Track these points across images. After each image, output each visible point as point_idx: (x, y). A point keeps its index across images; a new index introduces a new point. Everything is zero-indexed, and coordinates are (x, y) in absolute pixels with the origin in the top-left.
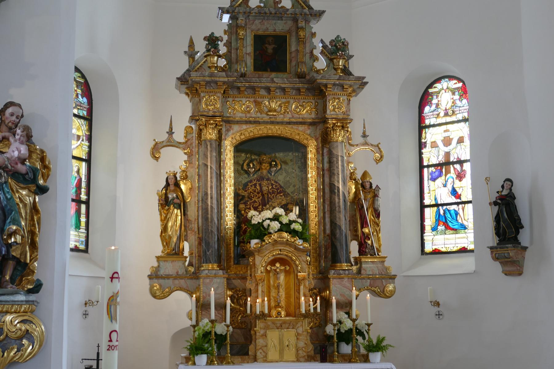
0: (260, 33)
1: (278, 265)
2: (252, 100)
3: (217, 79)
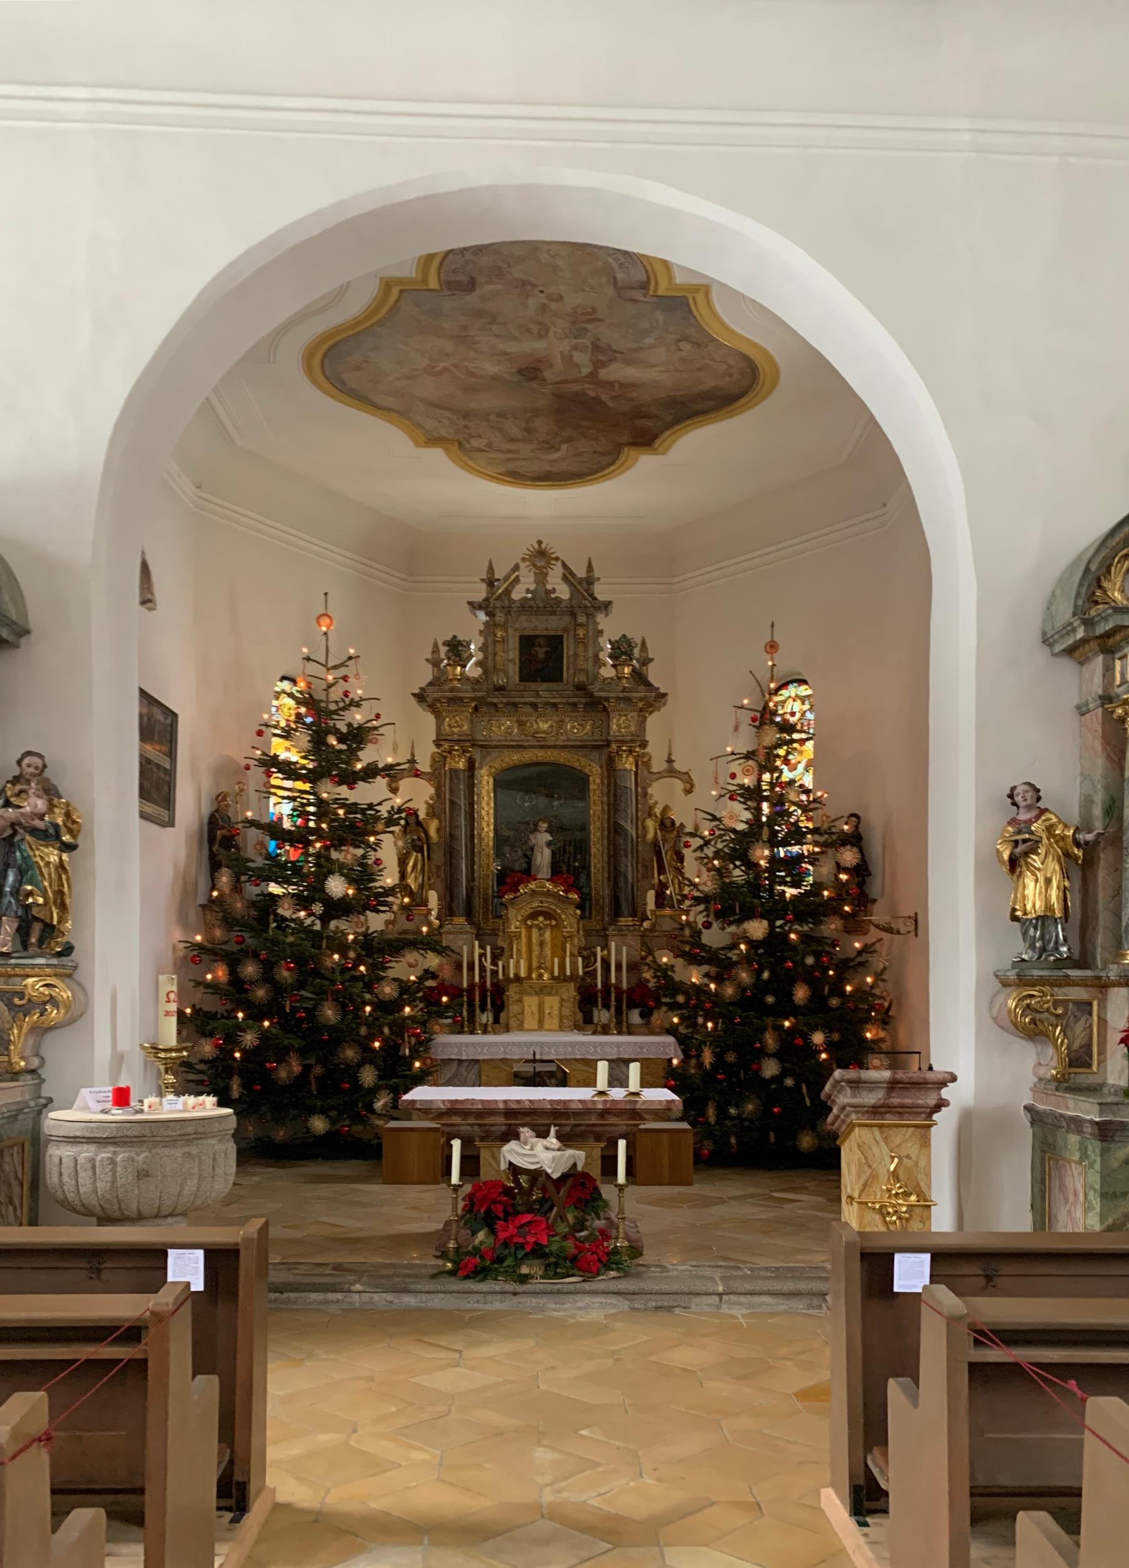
0: (527, 633)
1: (541, 919)
2: (514, 719)
3: (462, 695)
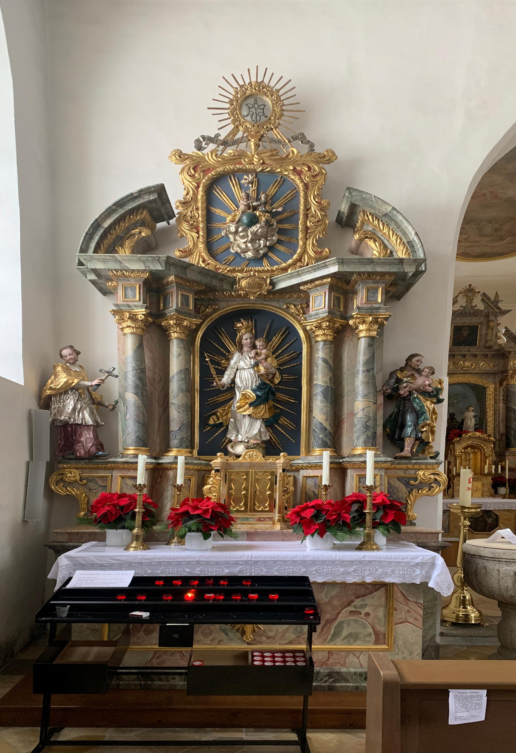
1: (469, 449)
